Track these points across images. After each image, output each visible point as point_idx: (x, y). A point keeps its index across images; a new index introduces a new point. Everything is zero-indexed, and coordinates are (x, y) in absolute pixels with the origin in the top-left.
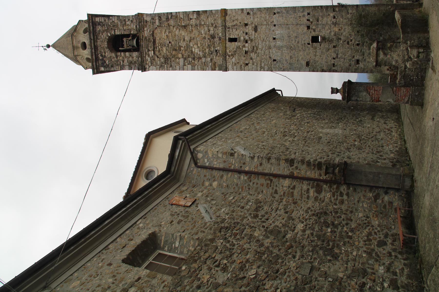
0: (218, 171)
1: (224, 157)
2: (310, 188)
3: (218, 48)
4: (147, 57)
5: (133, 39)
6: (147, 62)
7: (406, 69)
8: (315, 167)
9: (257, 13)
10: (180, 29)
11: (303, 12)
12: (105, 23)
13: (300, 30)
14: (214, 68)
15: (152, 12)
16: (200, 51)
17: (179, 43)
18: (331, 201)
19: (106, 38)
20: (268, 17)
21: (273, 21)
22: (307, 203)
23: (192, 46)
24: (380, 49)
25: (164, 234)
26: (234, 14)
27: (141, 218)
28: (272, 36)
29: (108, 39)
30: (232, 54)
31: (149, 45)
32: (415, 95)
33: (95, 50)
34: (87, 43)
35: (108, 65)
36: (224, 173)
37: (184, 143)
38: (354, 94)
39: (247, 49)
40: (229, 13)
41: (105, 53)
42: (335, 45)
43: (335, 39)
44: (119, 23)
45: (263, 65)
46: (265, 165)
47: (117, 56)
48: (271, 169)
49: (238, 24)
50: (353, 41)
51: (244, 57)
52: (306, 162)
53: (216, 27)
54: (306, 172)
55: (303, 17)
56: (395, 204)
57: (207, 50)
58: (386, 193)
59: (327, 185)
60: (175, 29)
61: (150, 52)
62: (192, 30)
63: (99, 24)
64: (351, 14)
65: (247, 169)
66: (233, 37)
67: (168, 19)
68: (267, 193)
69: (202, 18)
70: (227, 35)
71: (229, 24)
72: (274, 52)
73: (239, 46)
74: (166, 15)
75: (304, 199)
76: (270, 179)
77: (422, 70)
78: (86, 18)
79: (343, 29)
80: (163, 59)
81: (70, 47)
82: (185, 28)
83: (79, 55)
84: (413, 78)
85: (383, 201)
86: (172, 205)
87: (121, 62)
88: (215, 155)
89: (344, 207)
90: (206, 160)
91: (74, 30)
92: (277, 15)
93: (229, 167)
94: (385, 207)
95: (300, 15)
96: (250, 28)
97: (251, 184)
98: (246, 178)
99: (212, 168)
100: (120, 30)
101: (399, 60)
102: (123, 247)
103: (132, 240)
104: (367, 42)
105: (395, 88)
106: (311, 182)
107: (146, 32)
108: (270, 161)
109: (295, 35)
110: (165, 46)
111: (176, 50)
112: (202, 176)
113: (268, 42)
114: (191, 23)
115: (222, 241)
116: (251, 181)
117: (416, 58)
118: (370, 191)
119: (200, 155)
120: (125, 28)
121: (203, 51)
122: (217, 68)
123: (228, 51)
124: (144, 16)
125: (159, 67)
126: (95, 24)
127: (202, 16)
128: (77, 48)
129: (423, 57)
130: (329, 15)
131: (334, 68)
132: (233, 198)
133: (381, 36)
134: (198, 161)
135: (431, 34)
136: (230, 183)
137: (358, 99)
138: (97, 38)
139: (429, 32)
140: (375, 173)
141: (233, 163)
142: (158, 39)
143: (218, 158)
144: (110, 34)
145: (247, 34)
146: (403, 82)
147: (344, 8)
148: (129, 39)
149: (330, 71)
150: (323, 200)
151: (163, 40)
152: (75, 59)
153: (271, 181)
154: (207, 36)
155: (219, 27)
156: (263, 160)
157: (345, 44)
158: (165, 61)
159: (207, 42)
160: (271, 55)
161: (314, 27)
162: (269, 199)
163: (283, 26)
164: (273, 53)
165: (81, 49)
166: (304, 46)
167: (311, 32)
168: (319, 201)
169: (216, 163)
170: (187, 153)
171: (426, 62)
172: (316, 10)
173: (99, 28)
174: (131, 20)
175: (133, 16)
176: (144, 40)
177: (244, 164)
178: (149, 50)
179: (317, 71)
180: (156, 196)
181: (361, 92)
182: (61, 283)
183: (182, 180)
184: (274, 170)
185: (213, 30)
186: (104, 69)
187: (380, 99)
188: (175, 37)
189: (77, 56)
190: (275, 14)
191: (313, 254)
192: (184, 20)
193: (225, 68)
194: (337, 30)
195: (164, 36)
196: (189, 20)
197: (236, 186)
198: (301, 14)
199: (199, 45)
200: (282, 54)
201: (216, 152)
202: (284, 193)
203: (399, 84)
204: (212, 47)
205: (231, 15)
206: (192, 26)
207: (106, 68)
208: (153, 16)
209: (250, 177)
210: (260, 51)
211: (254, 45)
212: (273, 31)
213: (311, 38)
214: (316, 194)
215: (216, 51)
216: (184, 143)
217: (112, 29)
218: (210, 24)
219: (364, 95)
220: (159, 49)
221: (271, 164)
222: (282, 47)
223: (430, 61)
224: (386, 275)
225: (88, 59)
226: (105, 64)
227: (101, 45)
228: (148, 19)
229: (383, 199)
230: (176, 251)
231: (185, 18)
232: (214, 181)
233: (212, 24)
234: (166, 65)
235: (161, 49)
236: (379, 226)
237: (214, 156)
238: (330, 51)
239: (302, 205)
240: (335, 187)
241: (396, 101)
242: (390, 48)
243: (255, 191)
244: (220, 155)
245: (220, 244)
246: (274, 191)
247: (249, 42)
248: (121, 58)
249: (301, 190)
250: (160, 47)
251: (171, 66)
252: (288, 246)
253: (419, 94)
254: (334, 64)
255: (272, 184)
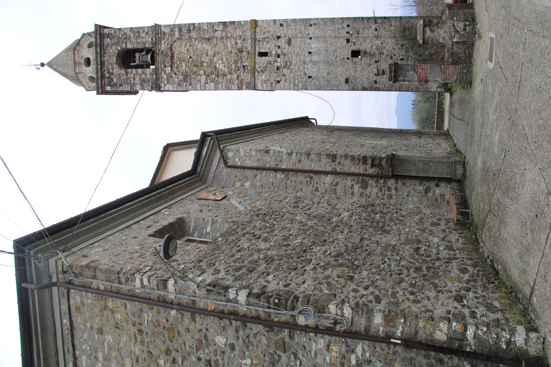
0: (251, 170)
1: (257, 155)
2: (355, 184)
3: (247, 63)
4: (163, 74)
5: (147, 53)
6: (163, 80)
7: (454, 47)
8: (360, 161)
9: (291, 24)
10: (203, 42)
11: (342, 24)
12: (115, 35)
13: (339, 44)
14: (240, 86)
15: (171, 23)
16: (225, 67)
17: (201, 58)
18: (378, 196)
19: (115, 52)
20: (303, 29)
21: (309, 34)
22: (352, 198)
23: (216, 61)
24: (426, 26)
25: (193, 219)
26: (265, 25)
27: (165, 208)
28: (307, 51)
29: (117, 54)
30: (262, 70)
31: (166, 61)
32: (463, 72)
33: (101, 66)
34: (92, 58)
35: (116, 84)
36: (258, 172)
37: (212, 141)
38: (401, 74)
39: (279, 65)
40: (259, 24)
41: (113, 70)
42: (377, 60)
43: (377, 53)
44: (132, 35)
45: (296, 82)
46: (305, 162)
47: (127, 74)
48: (311, 166)
49: (269, 36)
50: (397, 56)
51: (276, 73)
52: (349, 157)
53: (244, 39)
54: (350, 167)
55: (342, 29)
56: (447, 197)
57: (233, 66)
58: (437, 186)
59: (373, 180)
60: (197, 42)
61: (167, 68)
62: (217, 44)
63: (108, 37)
64: (394, 26)
65: (284, 166)
66: (264, 51)
67: (189, 31)
68: (306, 191)
69: (229, 29)
70: (257, 49)
71: (259, 37)
72: (309, 67)
73: (270, 61)
74: (187, 26)
75: (349, 196)
76: (310, 176)
77: (469, 47)
78: (93, 29)
79: (386, 43)
80: (182, 76)
81: (71, 63)
82: (209, 41)
83: (81, 73)
84: (461, 56)
85: (434, 194)
86: (200, 199)
87: (132, 80)
88: (248, 153)
89: (392, 201)
90: (237, 160)
91: (78, 43)
92: (313, 27)
93: (264, 165)
94: (436, 200)
95: (339, 27)
96: (283, 41)
97: (289, 182)
98: (282, 176)
99: (244, 168)
100: (132, 43)
101: (446, 36)
102: (148, 227)
103: (158, 222)
104: (411, 57)
105: (443, 66)
106: (356, 178)
107: (163, 46)
108: (310, 157)
109: (333, 48)
110: (185, 61)
111: (197, 66)
112: (233, 177)
113: (302, 57)
114: (216, 35)
115: (260, 222)
116: (288, 179)
117: (463, 31)
118: (421, 184)
119: (230, 154)
120: (138, 42)
121: (228, 67)
122: (244, 87)
123: (257, 66)
124: (162, 27)
125: (176, 85)
126: (104, 36)
127: (229, 27)
128: (80, 64)
129: (470, 29)
130: (370, 27)
131: (376, 85)
132: (269, 195)
133: (427, 50)
134: (228, 161)
135: (476, 10)
136: (264, 182)
137: (405, 79)
138: (104, 52)
139: (474, 8)
140: (424, 161)
141: (268, 161)
142: (177, 53)
143: (251, 156)
144: (121, 48)
145: (279, 47)
146: (450, 60)
147: (387, 19)
148: (143, 54)
149: (372, 89)
150: (369, 195)
151: (183, 54)
152: (76, 79)
153: (311, 178)
154: (233, 50)
155: (248, 40)
156: (302, 156)
157: (388, 59)
158: (184, 78)
159: (233, 57)
160: (306, 71)
161: (354, 40)
162: (309, 196)
163: (320, 39)
164: (308, 69)
165: (84, 66)
166: (343, 61)
167: (350, 45)
168: (365, 197)
169: (248, 162)
170: (215, 152)
171: (473, 35)
172: (356, 21)
173: (107, 41)
174: (146, 31)
175: (148, 27)
176: (160, 54)
177: (280, 161)
178: (165, 66)
179: (358, 90)
180: (181, 192)
181: (408, 71)
182: (82, 249)
183: (209, 181)
184: (314, 166)
185: (241, 43)
186: (111, 88)
187: (428, 79)
188: (197, 51)
189: (79, 73)
190: (311, 25)
191: (362, 230)
192: (208, 32)
193: (253, 86)
194: (379, 43)
195: (184, 50)
196: (214, 32)
197: (271, 185)
198: (340, 26)
199: (224, 60)
200: (318, 70)
201: (249, 150)
202: (326, 190)
203: (447, 62)
204: (239, 63)
205: (262, 27)
206: (217, 38)
207: (113, 87)
208: (172, 28)
209: (287, 175)
210: (294, 67)
211: (287, 59)
212: (309, 44)
213: (350, 52)
214: (361, 190)
215: (244, 66)
216: (212, 141)
217: (123, 41)
218: (238, 37)
219: (411, 74)
220: (177, 65)
221: (311, 160)
222: (318, 62)
223: (476, 34)
224: (441, 242)
225: (92, 79)
226: (112, 83)
227: (108, 61)
228: (167, 30)
229: (434, 192)
230: (208, 237)
231: (209, 29)
232: (247, 181)
233: (240, 37)
234: (184, 83)
235: (179, 65)
236: (431, 214)
237: (247, 154)
238: (372, 66)
239: (347, 200)
240: (382, 181)
241: (444, 80)
242: (437, 25)
243: (293, 189)
244: (253, 153)
245: (259, 224)
246: (314, 189)
247: (282, 56)
248: (132, 76)
249: (345, 186)
250: (178, 63)
251: (191, 84)
252: (334, 225)
253: (467, 71)
254: (376, 81)
255: (312, 182)
